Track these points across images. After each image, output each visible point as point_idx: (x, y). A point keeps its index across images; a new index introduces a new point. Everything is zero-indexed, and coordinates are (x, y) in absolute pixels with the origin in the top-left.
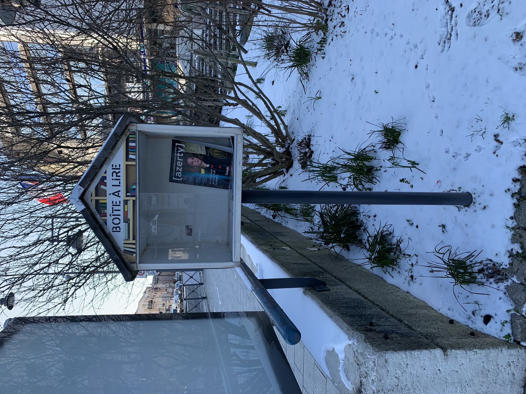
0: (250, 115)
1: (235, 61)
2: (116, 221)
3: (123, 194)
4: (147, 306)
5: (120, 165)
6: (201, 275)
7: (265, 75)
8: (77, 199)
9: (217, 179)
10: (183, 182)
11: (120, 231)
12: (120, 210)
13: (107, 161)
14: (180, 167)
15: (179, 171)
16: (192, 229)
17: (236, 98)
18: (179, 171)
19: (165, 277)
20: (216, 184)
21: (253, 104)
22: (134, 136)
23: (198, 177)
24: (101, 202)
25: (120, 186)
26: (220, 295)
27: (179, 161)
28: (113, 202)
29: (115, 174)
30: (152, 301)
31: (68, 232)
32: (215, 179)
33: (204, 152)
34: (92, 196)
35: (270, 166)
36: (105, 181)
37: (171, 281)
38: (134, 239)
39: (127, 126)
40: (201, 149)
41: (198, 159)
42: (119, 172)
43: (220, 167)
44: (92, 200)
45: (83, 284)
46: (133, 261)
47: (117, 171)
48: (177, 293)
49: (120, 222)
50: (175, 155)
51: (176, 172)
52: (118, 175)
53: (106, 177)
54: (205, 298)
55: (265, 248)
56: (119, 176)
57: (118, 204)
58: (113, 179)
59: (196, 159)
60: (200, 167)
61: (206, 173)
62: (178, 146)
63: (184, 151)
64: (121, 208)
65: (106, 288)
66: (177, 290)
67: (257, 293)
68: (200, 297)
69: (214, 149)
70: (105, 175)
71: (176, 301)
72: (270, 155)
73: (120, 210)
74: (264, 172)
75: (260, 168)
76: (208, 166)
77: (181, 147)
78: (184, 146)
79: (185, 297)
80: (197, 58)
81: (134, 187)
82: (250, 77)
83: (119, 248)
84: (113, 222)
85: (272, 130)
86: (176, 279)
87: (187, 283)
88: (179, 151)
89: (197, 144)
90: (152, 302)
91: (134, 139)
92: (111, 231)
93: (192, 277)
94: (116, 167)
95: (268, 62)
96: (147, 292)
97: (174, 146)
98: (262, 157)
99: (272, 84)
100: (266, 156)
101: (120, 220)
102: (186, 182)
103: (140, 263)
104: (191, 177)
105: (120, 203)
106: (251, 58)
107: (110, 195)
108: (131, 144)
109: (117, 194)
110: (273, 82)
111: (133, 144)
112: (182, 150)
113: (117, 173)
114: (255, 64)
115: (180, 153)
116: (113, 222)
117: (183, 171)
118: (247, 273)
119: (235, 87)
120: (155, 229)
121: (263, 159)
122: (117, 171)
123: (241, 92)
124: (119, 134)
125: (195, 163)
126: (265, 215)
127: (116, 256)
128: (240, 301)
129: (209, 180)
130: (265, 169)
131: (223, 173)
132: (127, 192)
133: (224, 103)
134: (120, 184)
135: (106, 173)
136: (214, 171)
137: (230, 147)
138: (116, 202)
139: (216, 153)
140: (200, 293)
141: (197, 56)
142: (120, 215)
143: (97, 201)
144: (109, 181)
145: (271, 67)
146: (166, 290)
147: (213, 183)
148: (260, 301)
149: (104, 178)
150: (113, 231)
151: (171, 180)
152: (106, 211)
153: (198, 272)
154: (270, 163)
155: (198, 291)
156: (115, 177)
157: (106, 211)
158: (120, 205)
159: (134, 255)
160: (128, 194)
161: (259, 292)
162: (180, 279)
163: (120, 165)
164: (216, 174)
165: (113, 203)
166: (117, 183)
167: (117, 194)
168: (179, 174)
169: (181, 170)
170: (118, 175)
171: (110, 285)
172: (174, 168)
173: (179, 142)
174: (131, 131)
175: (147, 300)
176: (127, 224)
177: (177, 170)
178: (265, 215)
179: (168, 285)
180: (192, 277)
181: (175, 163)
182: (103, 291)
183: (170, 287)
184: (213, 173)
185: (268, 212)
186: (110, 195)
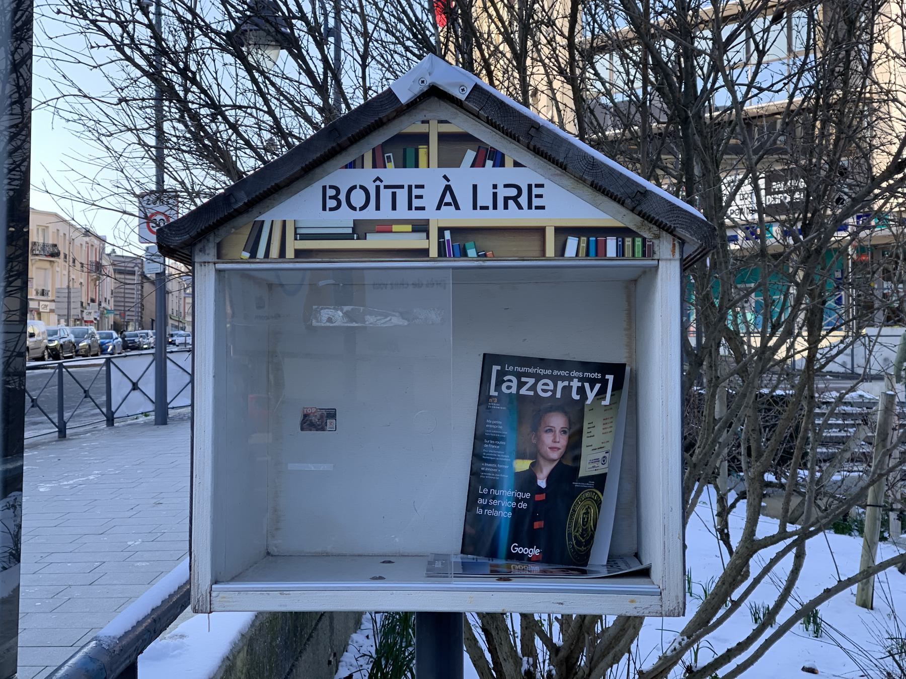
0: (693, 585)
1: (873, 533)
2: (358, 198)
3: (449, 217)
4: (41, 241)
5: (543, 208)
6: (142, 419)
7: (834, 640)
8: (429, 80)
9: (497, 514)
10: (484, 399)
11: (324, 209)
12: (394, 208)
13: (558, 171)
14: (533, 388)
15: (521, 385)
16: (323, 429)
17: (752, 545)
18: (521, 385)
19: (136, 296)
20: (479, 511)
21: (736, 604)
22: (638, 253)
23: (503, 448)
24: (422, 151)
25: (475, 208)
26: (72, 487)
27: (555, 386)
28: (422, 187)
29: (513, 192)
30: (56, 254)
31: (303, 18)
32: (498, 508)
33: (585, 470)
34: (441, 122)
35: (525, 667)
36: (489, 163)
37: (123, 315)
38: (299, 253)
39: (671, 231)
40: (597, 460)
41: (562, 450)
42: (520, 207)
43: (537, 525)
44: (428, 122)
45: (129, 59)
46: (224, 252)
47: (524, 200)
48: (80, 336)
49: (354, 209)
50: (574, 373)
51: (519, 376)
52: (511, 203)
53: (502, 165)
54: (62, 433)
55: (239, 663)
56: (506, 207)
57: (416, 203)
58: (495, 187)
59: (563, 441)
60: (535, 456)
61: (518, 474)
62: (605, 383)
63: (589, 402)
64: (403, 212)
65: (112, 129)
66: (92, 335)
67: (90, 658)
68: (67, 415)
69: (599, 503)
70: (509, 161)
71: (55, 333)
72: (564, 668)
73: (394, 208)
74: (506, 649)
75: (518, 629)
76: (542, 483)
77: (602, 392)
78: (607, 402)
79: (64, 364)
80: (861, 396)
81: (472, 253)
82: (828, 593)
83: (269, 208)
84: (354, 187)
85: (650, 672)
86: (131, 330)
87: (115, 373)
88: (587, 385)
89: (614, 447)
90: (52, 255)
91: (628, 252)
92: (327, 181)
93: (135, 387)
94: (537, 196)
95: (878, 652)
96: (87, 239)
97: (605, 368)
98: (557, 639)
99: (807, 665)
100: (562, 654)
101: (362, 209)
102: (483, 407)
103: (219, 272)
104: (501, 425)
105: (417, 208)
106: (885, 586)
107: (445, 177)
108: (611, 244)
109: (448, 199)
110: (812, 671)
111: (611, 250)
112: (591, 396)
113: (515, 199)
114: (866, 603)
115: (581, 390)
116: (354, 187)
117: (521, 398)
118: (159, 612)
119: (789, 541)
120: (330, 320)
121: (547, 641)
122: (524, 200)
123: (774, 562)
124: (645, 208)
125: (548, 439)
126: (350, 648)
127: (243, 198)
128: (48, 560)
129: (495, 485)
130: (513, 649)
131: (516, 536)
132: (454, 230)
133: (725, 494)
134: (482, 208)
135: (517, 164)
136: (524, 505)
137: (612, 560)
138: (420, 197)
139: (587, 513)
140: (79, 415)
141: (877, 398)
142: (378, 208)
143: (424, 138)
144: (488, 175)
145: (863, 661)
146: (93, 301)
147: (481, 501)
148: (66, 668)
149: (499, 161)
150: (324, 188)
151: (488, 360)
152: (390, 165)
153: (150, 407)
154: (535, 665)
155: (87, 408)
156: (502, 193)
157: (390, 165)
158: (410, 208)
159: (246, 255)
160: (447, 235)
161: (93, 666)
162: (130, 346)
163: (543, 208)
164: (515, 510)
165: (417, 187)
166: (485, 198)
167: (448, 199)
168: (511, 386)
169: (523, 391)
170: (511, 203)
171: (122, 142)
172: (531, 370)
173: (618, 386)
174: (656, 242)
175: (61, 239)
176: (350, 231)
177: (523, 379)
178: (351, 648)
179: (111, 306)
180: (135, 387)
181: (549, 372)
182: (103, 118)
183: (102, 314)
184: (517, 500)
185: (362, 661)
186: (445, 177)
